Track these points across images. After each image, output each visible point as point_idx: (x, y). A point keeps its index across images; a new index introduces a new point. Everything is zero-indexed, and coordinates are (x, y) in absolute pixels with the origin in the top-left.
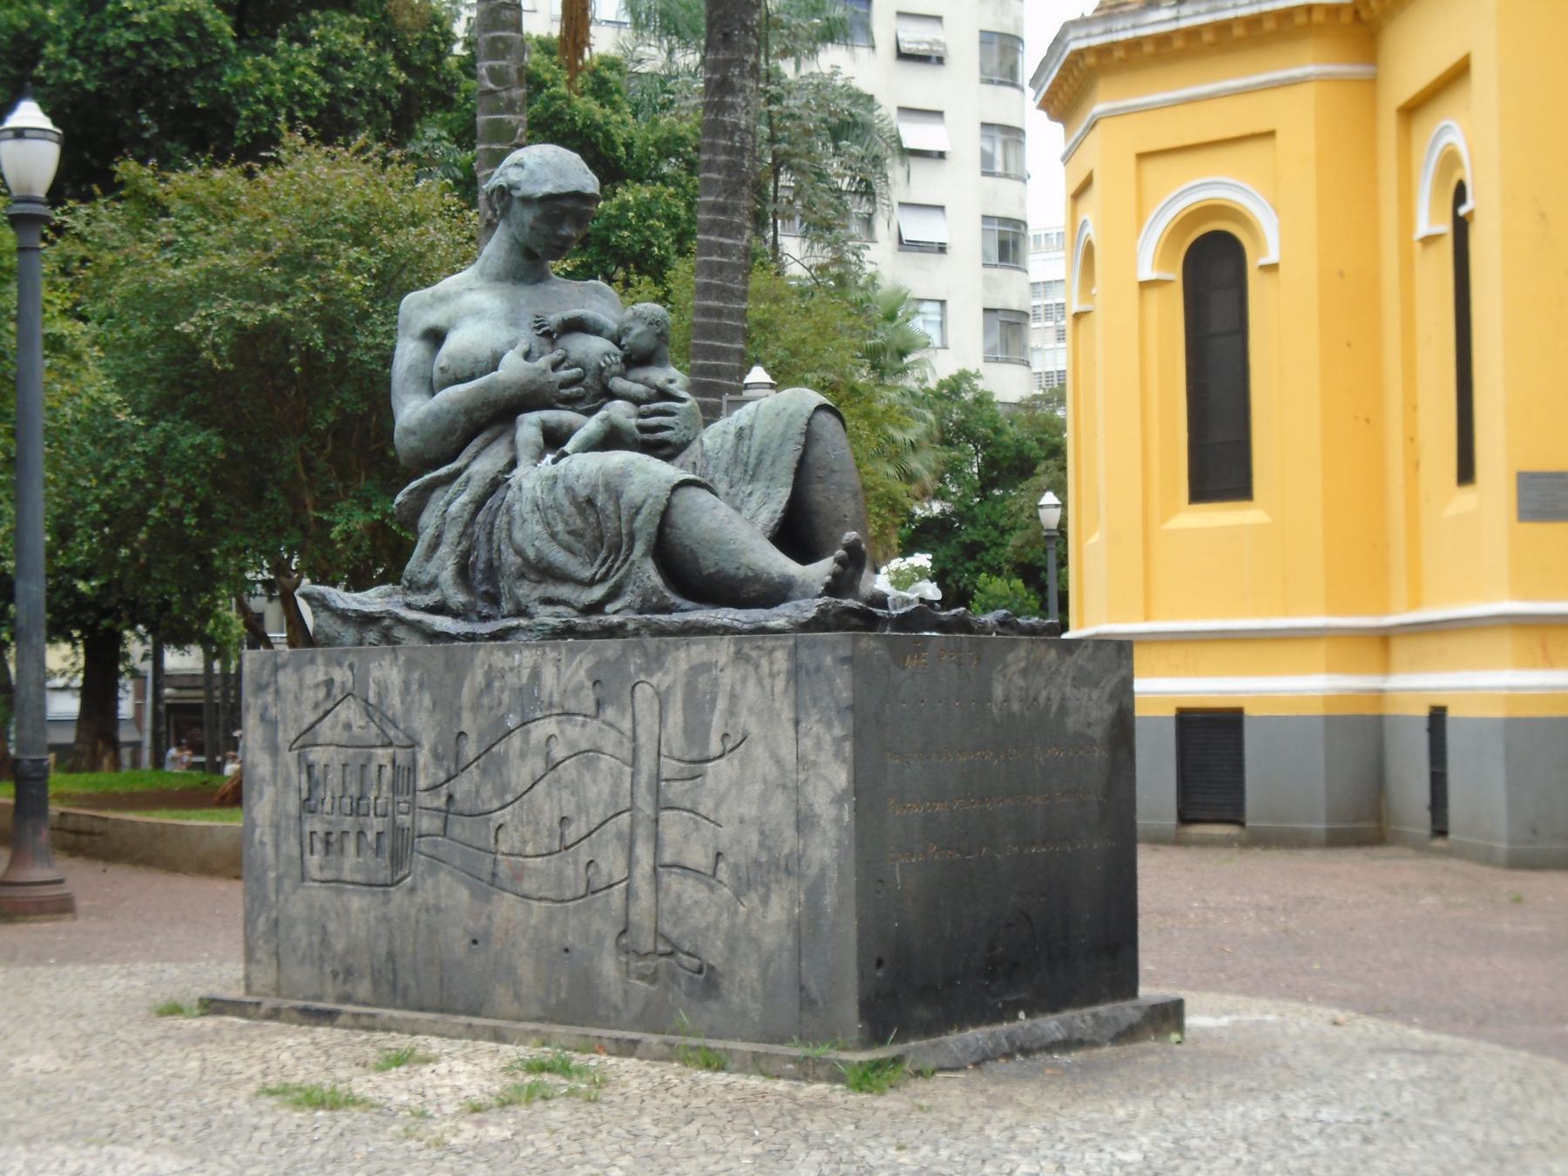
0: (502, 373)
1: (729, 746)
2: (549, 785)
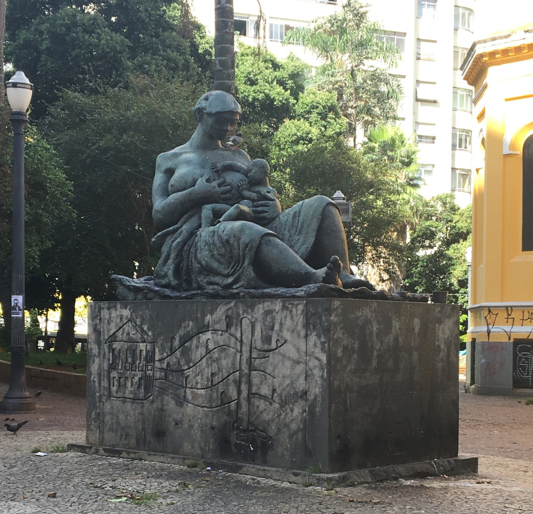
1: (279, 345)
2: (207, 360)
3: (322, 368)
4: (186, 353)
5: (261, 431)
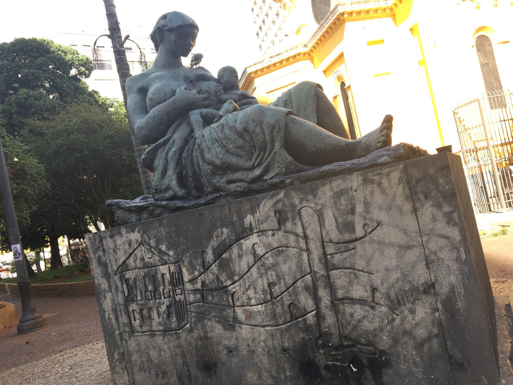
1: (369, 230)
2: (258, 268)
4: (225, 266)
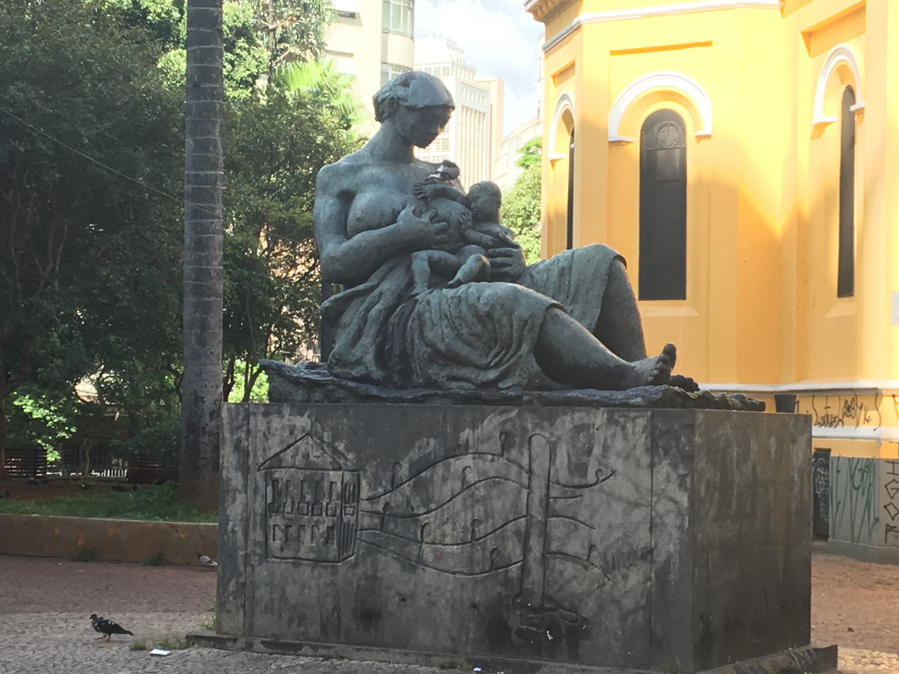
0: (400, 222)
1: (601, 478)
2: (464, 499)
3: (681, 515)
4: (422, 487)
5: (567, 610)
